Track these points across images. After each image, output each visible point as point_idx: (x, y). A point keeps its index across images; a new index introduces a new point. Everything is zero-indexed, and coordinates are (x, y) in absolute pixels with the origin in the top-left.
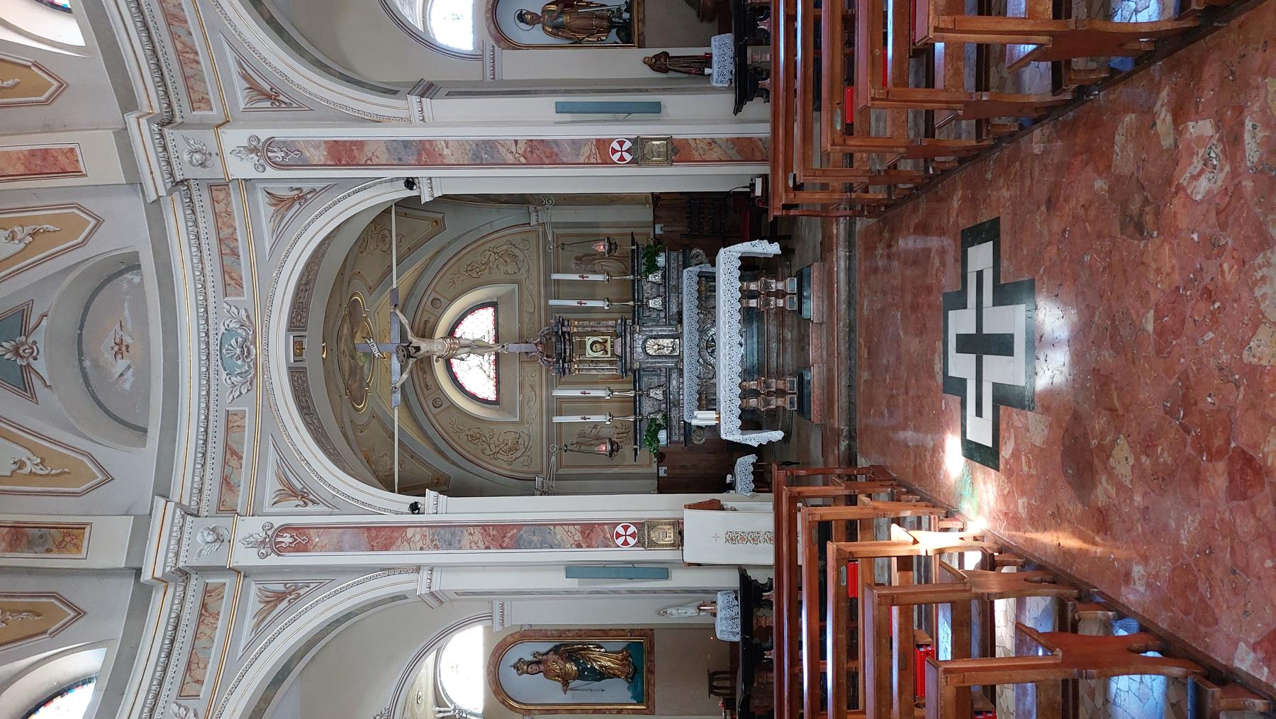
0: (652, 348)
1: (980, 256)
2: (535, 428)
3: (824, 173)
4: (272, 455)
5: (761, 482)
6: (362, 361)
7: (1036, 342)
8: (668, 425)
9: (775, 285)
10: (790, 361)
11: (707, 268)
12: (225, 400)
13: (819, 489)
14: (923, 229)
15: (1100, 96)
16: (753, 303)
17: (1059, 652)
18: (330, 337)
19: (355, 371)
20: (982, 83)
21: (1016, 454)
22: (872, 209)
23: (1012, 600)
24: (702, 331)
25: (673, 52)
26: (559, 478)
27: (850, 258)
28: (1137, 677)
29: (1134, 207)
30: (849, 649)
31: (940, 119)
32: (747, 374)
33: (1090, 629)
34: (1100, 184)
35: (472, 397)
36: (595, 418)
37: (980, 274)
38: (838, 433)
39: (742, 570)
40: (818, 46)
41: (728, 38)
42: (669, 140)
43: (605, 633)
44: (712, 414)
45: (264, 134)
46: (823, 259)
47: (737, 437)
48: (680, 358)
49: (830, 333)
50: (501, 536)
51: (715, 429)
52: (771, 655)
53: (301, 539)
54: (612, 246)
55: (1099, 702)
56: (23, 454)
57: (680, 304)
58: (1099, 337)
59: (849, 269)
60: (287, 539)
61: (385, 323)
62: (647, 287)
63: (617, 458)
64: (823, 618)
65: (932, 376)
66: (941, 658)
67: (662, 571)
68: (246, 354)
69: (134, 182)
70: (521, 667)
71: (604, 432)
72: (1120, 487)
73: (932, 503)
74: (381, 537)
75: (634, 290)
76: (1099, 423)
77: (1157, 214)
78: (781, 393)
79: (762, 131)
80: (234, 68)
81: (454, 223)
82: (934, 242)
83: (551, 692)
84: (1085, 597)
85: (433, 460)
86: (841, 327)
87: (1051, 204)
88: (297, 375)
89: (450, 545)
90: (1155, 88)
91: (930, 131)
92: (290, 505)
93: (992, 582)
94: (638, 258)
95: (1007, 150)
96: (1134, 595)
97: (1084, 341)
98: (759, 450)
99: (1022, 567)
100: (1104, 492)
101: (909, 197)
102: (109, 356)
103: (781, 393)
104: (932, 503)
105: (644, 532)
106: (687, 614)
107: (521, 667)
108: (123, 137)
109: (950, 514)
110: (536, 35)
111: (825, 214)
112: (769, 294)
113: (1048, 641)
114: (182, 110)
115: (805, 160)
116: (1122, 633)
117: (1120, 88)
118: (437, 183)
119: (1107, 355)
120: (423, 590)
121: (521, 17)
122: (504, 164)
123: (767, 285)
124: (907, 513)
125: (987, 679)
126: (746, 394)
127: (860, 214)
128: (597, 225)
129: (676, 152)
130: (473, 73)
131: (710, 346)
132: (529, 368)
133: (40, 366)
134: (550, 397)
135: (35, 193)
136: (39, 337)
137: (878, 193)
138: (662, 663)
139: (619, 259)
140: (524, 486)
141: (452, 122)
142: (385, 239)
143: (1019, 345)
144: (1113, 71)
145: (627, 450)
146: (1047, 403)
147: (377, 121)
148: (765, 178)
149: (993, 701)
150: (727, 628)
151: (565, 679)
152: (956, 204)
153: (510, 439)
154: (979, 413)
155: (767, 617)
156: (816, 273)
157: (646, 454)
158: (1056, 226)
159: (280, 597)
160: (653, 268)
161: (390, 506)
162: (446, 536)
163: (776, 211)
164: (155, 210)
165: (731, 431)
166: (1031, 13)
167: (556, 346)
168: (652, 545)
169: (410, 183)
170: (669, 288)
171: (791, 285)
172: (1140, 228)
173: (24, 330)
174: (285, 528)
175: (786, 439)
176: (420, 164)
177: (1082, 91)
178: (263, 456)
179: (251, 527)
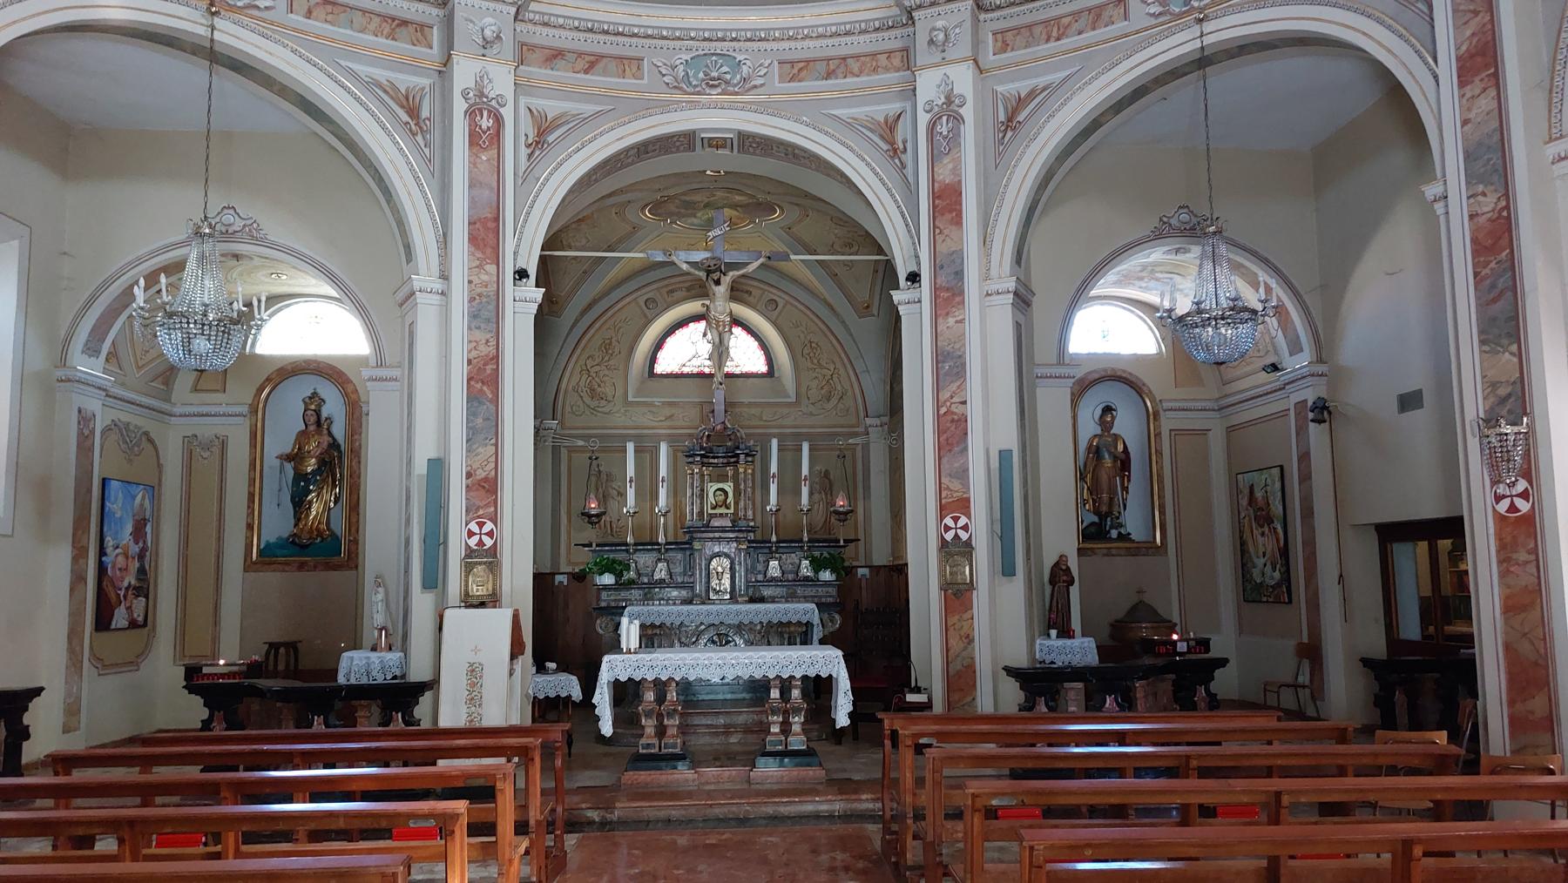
2: (618, 419)
3: (937, 784)
4: (589, 108)
5: (546, 708)
6: (704, 215)
8: (621, 585)
9: (797, 721)
10: (701, 741)
11: (818, 633)
16: (775, 694)
18: (732, 182)
22: (894, 845)
24: (739, 628)
25: (1074, 591)
26: (556, 450)
27: (831, 817)
30: (322, 831)
32: (685, 687)
35: (659, 345)
36: (631, 494)
38: (609, 808)
39: (432, 685)
40: (1088, 774)
41: (1092, 659)
42: (971, 586)
43: (354, 507)
45: (967, 112)
47: (605, 676)
48: (706, 600)
50: (485, 379)
51: (615, 647)
52: (318, 726)
53: (486, 139)
54: (843, 516)
57: (773, 600)
59: (817, 817)
60: (486, 122)
61: (748, 244)
62: (794, 558)
67: (434, 580)
68: (712, 83)
70: (314, 402)
71: (613, 505)
74: (486, 235)
75: (791, 542)
78: (661, 731)
79: (985, 703)
80: (1041, 81)
81: (868, 329)
83: (279, 441)
85: (582, 297)
86: (744, 808)
88: (686, 141)
89: (474, 316)
92: (528, 129)
94: (829, 545)
98: (587, 705)
103: (661, 731)
105: (485, 557)
106: (376, 612)
107: (314, 402)
110: (1089, 427)
111: (886, 784)
112: (786, 713)
115: (953, 759)
118: (915, 308)
120: (418, 281)
121: (1108, 410)
122: (938, 388)
123: (797, 711)
126: (660, 686)
129: (957, 595)
130: (1043, 352)
131: (721, 639)
132: (694, 413)
137: (913, 853)
138: (314, 581)
140: (547, 406)
141: (987, 329)
142: (848, 247)
145: (590, 534)
147: (985, 241)
148: (928, 706)
150: (356, 666)
151: (296, 457)
153: (608, 390)
156: (813, 773)
157: (584, 558)
159: (413, 112)
160: (817, 565)
161: (524, 244)
162: (486, 312)
163: (889, 721)
165: (612, 668)
167: (721, 445)
168: (468, 568)
169: (914, 278)
170: (793, 586)
171: (797, 742)
174: (499, 121)
175: (601, 739)
176: (936, 290)
179: (501, 81)
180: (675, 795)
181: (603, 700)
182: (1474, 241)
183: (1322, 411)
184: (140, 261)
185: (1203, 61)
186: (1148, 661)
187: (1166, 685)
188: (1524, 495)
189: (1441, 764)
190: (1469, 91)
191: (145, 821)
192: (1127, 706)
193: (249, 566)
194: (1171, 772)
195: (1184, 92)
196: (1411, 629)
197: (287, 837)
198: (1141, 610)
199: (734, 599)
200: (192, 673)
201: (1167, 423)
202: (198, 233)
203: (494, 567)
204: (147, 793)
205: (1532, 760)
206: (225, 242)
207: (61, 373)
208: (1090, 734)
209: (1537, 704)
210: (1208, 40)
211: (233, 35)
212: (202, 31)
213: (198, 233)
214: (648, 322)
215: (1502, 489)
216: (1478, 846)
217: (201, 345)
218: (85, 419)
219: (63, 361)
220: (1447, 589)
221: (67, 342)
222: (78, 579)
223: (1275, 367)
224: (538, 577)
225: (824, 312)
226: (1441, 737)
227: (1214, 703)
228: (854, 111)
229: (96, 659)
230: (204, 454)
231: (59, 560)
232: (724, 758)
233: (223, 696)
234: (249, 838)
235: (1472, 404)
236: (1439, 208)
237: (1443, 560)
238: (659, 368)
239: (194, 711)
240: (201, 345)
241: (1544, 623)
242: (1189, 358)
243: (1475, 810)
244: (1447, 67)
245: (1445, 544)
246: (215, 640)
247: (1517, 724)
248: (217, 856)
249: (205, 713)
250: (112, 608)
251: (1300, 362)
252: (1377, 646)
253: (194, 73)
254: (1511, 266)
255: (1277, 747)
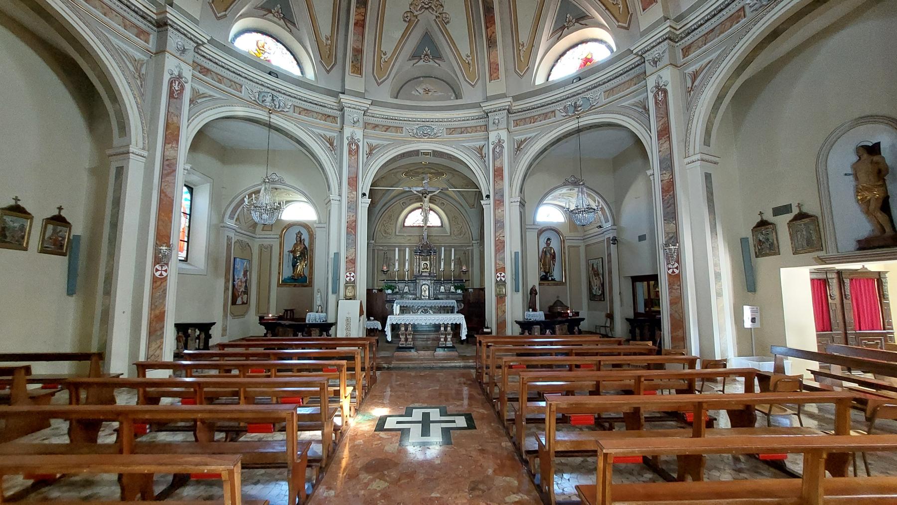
0: (425, 287)
1: (461, 422)
2: (393, 240)
3: (493, 358)
4: (386, 143)
5: (370, 332)
6: (421, 176)
7: (424, 446)
8: (394, 293)
9: (449, 337)
10: (419, 343)
11: (456, 310)
12: (407, 127)
13: (368, 355)
14: (471, 398)
15: (524, 470)
16: (442, 329)
17: (299, 461)
18: (431, 165)
19: (417, 174)
20: (529, 421)
21: (381, 438)
22: (479, 376)
23: (321, 438)
24: (431, 308)
25: (537, 296)
26: (373, 250)
27: (460, 367)
28: (287, 493)
29: (481, 486)
30: (301, 369)
31: (515, 404)
32: (414, 326)
33: (308, 472)
34: (490, 471)
35: (406, 217)
36: (397, 264)
37: (454, 422)
38: (390, 363)
39: (335, 324)
40: (541, 355)
41: (543, 318)
42: (505, 295)
43: (311, 267)
44: (398, 312)
45: (505, 145)
46: (460, 356)
47: (389, 322)
48: (420, 299)
49: (429, 360)
50: (352, 228)
51: (392, 313)
52: (300, 336)
53: (354, 153)
54: (465, 272)
55: (277, 477)
56: (389, 55)
57: (442, 299)
58: (428, 473)
59: (455, 367)
60: (354, 147)
61: (435, 185)
62: (449, 286)
63: (380, 273)
64: (315, 359)
65: (413, 402)
66: (298, 409)
67: (335, 291)
68: (425, 135)
69: (487, 99)
70: (299, 234)
71: (391, 267)
72: (367, 485)
73: (361, 403)
74: (353, 182)
75: (448, 280)
76: (394, 474)
77: (478, 496)
78: (406, 340)
79: (509, 332)
80: (528, 136)
81: (473, 212)
82: (466, 402)
83: (289, 245)
84: (321, 470)
85: (383, 202)
86: (432, 364)
87: (482, 451)
88: (416, 153)
89: (349, 208)
90: (528, 493)
91: (510, 400)
92: (367, 149)
93: (328, 429)
94: (460, 283)
95: (503, 432)
96: (322, 491)
97: (427, 465)
98: (383, 331)
99: (334, 442)
100: (365, 477)
101: (484, 391)
102: (424, 87)
103: (406, 340)
104: (361, 403)
105: (351, 284)
106: (318, 301)
107: (299, 234)
108: (504, 96)
109: (357, 411)
110: (543, 245)
111: (477, 357)
112: (446, 335)
113: (303, 456)
114: (513, 117)
115: (499, 350)
116: (306, 487)
117: (527, 478)
118: (488, 206)
119: (422, 477)
120: (332, 197)
121: (549, 239)
122: (495, 232)
123: (449, 334)
124: (357, 393)
125: (289, 429)
126: (406, 326)
127: (477, 371)
128: (472, 266)
129: (501, 298)
130: (528, 221)
131: (425, 311)
132: (417, 238)
133: (421, 63)
134: (406, 247)
135: (484, 65)
136: (432, 63)
137: (486, 379)
138: (298, 290)
139: (460, 274)
140: (371, 236)
141: (511, 213)
142: (467, 186)
143: (425, 439)
144: (534, 475)
145: (384, 277)
146: (402, 451)
147: (511, 185)
148: (491, 333)
149: (280, 431)
150: (312, 317)
151: (293, 252)
152: (481, 411)
153: (390, 231)
154: (398, 423)
155: (315, 334)
156: (455, 353)
157: (382, 285)
158: (474, 454)
159: (331, 144)
160: (456, 288)
161: (365, 185)
162: (353, 207)
163: (478, 338)
164: (477, 105)
165: (391, 320)
166: (557, 442)
167: (426, 247)
168: (346, 287)
169: (488, 196)
170: (448, 295)
171: (449, 344)
172: (473, 489)
173: (434, 58)
174: (358, 146)
175: (387, 342)
176: (495, 201)
177: (526, 462)
178: (386, 139)
179: (359, 134)
180: (411, 360)
181: (388, 329)
182: (662, 188)
183: (615, 240)
184: (246, 190)
185: (579, 131)
186: (560, 319)
187: (566, 326)
188: (677, 268)
189: (650, 352)
190: (661, 142)
191: (248, 365)
192: (553, 333)
193: (279, 285)
194: (567, 354)
195: (573, 139)
196: (641, 309)
197: (290, 370)
198: (558, 303)
199: (429, 299)
200: (261, 318)
201: (567, 244)
202: (264, 182)
203: (354, 287)
204: (247, 356)
205: (677, 351)
206: (273, 184)
207: (222, 225)
208: (541, 342)
209: (680, 333)
210: (580, 124)
211: (276, 120)
212: (267, 118)
213: (264, 182)
214: (403, 210)
215: (670, 266)
216: (660, 377)
217: (265, 216)
218: (229, 239)
219: (222, 222)
220: (652, 296)
221: (223, 217)
222: (226, 289)
223: (600, 227)
224: (368, 290)
225: (459, 207)
226: (650, 343)
227: (580, 332)
228: (319, 131)
229: (232, 313)
230: (265, 250)
231: (221, 282)
232: (426, 348)
233: (271, 327)
234: (279, 371)
235: (661, 239)
236: (651, 178)
237: (651, 287)
238: (406, 224)
239: (262, 330)
240: (265, 216)
241: (682, 308)
242: (575, 225)
243: (660, 366)
244: (654, 135)
245: (652, 283)
246: (268, 308)
247: (673, 339)
248: (269, 376)
249: (265, 331)
250: (237, 298)
251: (608, 225)
252: (631, 315)
253: (265, 130)
254: (674, 197)
255: (599, 346)
